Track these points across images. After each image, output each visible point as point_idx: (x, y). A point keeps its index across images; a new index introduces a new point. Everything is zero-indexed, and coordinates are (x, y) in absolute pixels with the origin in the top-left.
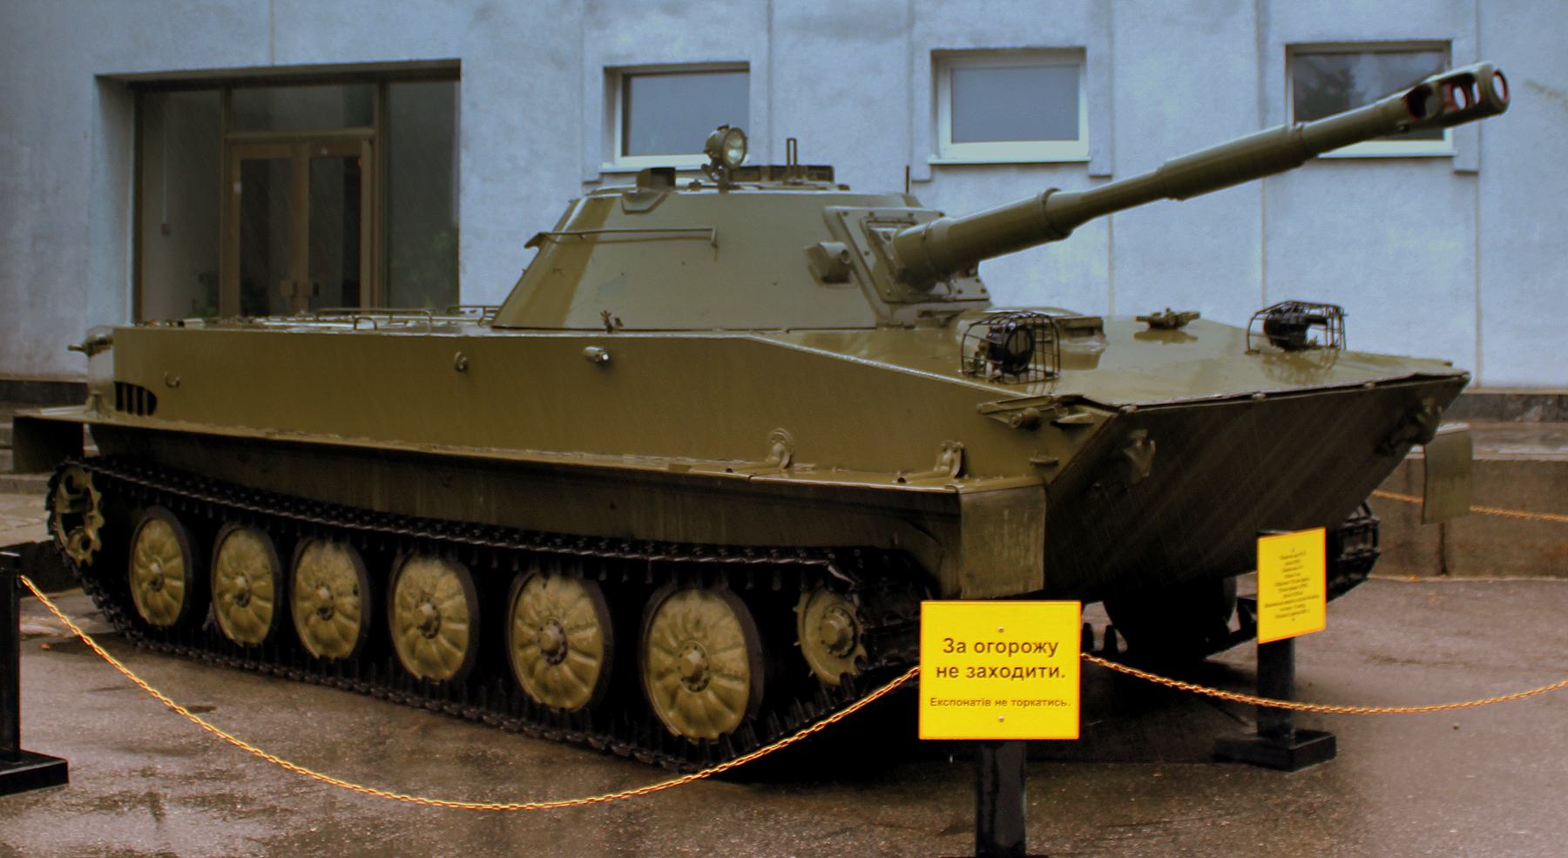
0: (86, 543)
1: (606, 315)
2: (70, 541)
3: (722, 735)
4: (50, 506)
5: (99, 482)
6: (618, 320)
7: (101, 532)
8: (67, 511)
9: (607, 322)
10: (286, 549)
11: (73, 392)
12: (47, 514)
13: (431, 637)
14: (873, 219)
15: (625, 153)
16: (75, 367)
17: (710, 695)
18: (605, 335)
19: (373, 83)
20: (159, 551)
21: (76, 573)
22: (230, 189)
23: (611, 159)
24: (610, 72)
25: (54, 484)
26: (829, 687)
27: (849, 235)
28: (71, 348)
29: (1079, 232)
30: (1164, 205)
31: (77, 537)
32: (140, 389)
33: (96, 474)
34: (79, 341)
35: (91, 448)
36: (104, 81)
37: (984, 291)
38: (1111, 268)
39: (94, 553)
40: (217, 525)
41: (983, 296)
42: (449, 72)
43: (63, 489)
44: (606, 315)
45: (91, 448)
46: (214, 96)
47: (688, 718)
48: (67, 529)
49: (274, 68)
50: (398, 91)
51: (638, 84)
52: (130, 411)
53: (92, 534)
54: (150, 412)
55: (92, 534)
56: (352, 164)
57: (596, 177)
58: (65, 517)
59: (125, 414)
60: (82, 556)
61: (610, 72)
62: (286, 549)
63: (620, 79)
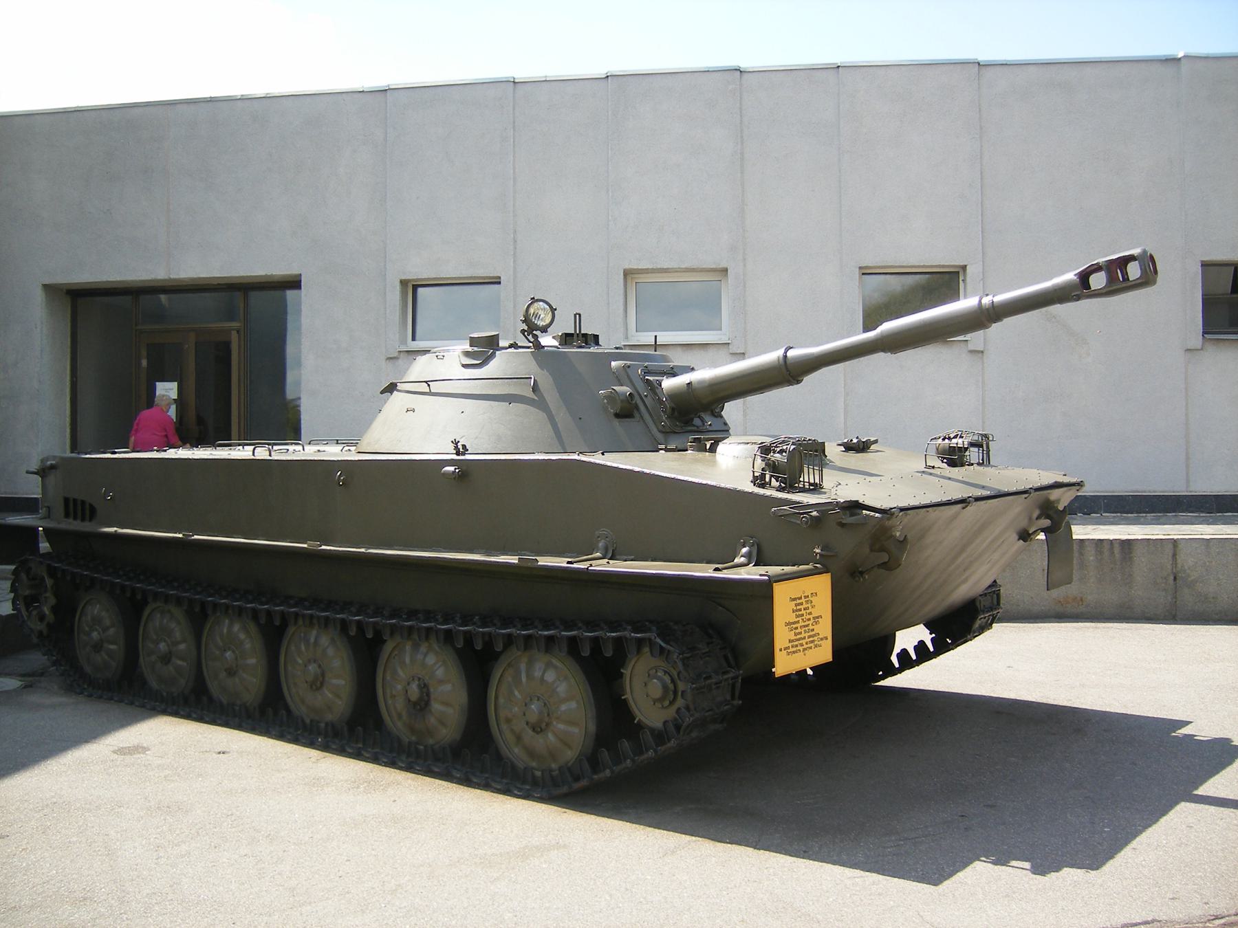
0: (42, 618)
1: (456, 443)
2: (29, 616)
3: (560, 768)
4: (13, 589)
5: (52, 572)
6: (464, 446)
7: (54, 609)
8: (27, 592)
9: (456, 448)
10: (199, 618)
11: (28, 505)
12: (12, 595)
13: (318, 689)
14: (648, 371)
15: (414, 339)
16: (31, 488)
17: (550, 736)
18: (455, 457)
19: (239, 292)
20: (99, 618)
21: (35, 640)
22: (140, 364)
23: (404, 342)
24: (404, 283)
25: (15, 572)
26: (652, 730)
27: (631, 381)
28: (28, 472)
29: (808, 380)
30: (880, 357)
31: (34, 613)
32: (83, 502)
33: (49, 566)
34: (34, 466)
35: (44, 546)
36: (48, 288)
37: (726, 424)
38: (745, 415)
39: (48, 625)
40: (145, 603)
41: (724, 428)
42: (294, 283)
43: (23, 576)
44: (456, 443)
45: (44, 546)
46: (126, 300)
47: (531, 754)
48: (28, 606)
49: (170, 280)
50: (254, 295)
51: (420, 290)
52: (75, 518)
53: (46, 610)
54: (91, 520)
55: (46, 610)
56: (225, 347)
57: (396, 355)
58: (26, 598)
59: (71, 520)
60: (41, 626)
61: (404, 283)
62: (199, 618)
63: (412, 288)
